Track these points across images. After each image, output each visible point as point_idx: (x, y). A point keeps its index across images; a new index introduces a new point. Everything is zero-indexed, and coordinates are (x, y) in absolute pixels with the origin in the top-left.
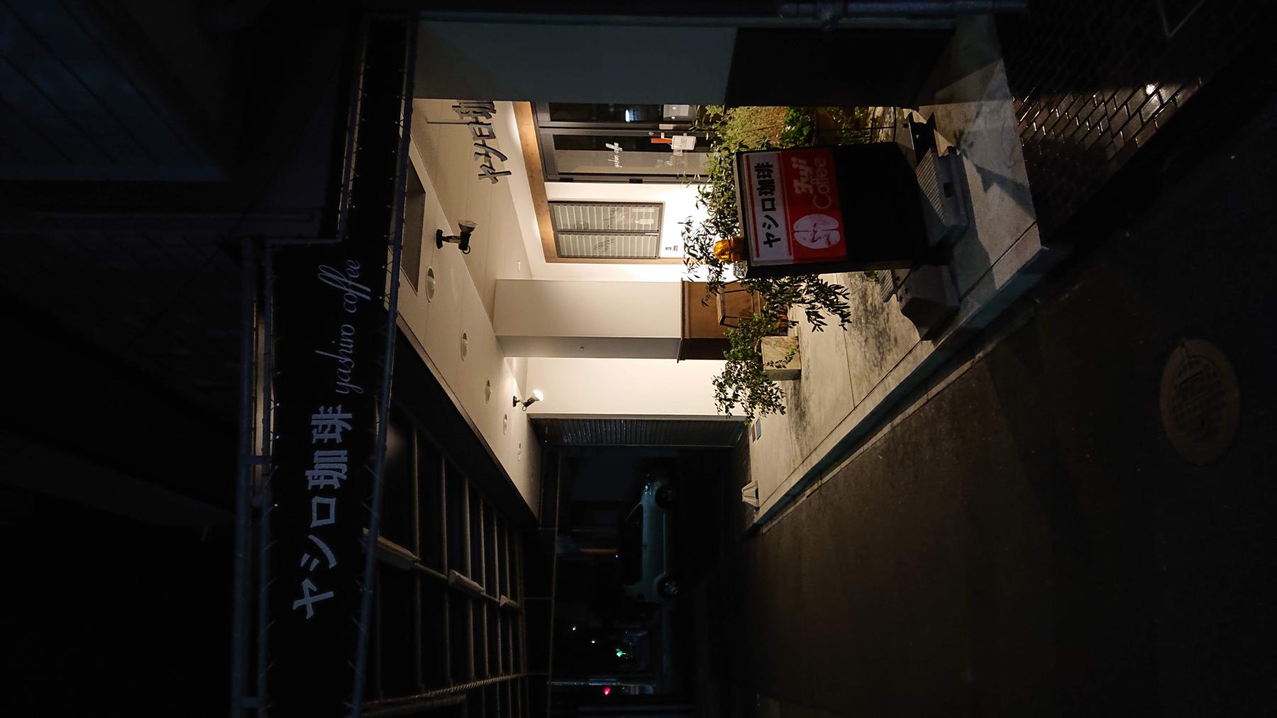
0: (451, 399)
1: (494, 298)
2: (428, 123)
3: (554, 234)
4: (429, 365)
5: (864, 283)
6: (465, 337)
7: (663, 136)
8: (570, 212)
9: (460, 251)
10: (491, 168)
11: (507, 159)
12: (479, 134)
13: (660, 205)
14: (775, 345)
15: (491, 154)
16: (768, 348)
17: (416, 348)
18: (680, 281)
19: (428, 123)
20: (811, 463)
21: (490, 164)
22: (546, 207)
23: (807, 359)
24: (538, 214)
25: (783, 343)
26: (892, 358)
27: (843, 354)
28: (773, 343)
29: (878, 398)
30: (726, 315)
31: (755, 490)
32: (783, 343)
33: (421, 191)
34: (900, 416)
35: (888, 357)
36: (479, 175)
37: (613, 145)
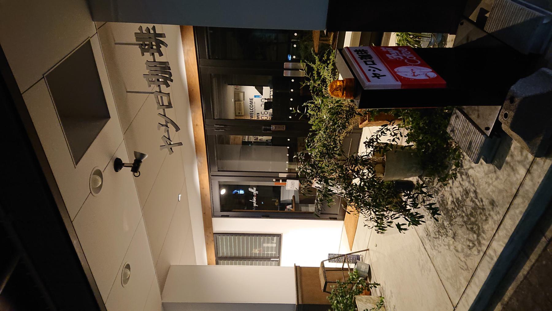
0: (80, 257)
1: (168, 271)
2: (128, 92)
3: (216, 260)
4: (75, 242)
5: (439, 194)
6: (128, 267)
7: (281, 181)
8: (226, 239)
9: (132, 173)
10: (169, 139)
11: (182, 145)
12: (161, 105)
13: (279, 236)
14: (365, 302)
15: (169, 125)
16: (360, 303)
17: (64, 219)
18: (293, 266)
19: (128, 92)
20: (495, 251)
21: (169, 136)
22: (211, 238)
23: (392, 306)
24: (207, 244)
25: (371, 301)
26: (489, 227)
27: (430, 271)
28: (364, 300)
29: (483, 275)
30: (328, 281)
31: (446, 250)
32: (371, 301)
33: (108, 117)
34: (510, 288)
35: (486, 227)
36: (159, 123)
37: (253, 189)
